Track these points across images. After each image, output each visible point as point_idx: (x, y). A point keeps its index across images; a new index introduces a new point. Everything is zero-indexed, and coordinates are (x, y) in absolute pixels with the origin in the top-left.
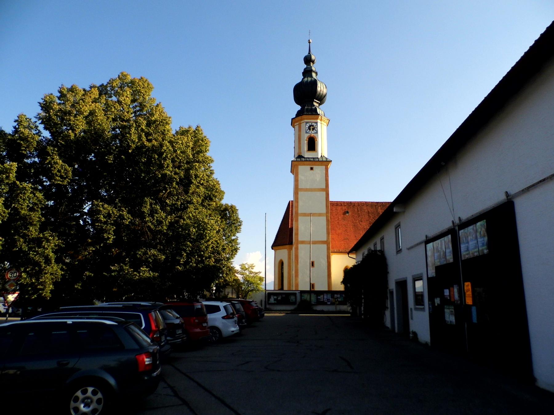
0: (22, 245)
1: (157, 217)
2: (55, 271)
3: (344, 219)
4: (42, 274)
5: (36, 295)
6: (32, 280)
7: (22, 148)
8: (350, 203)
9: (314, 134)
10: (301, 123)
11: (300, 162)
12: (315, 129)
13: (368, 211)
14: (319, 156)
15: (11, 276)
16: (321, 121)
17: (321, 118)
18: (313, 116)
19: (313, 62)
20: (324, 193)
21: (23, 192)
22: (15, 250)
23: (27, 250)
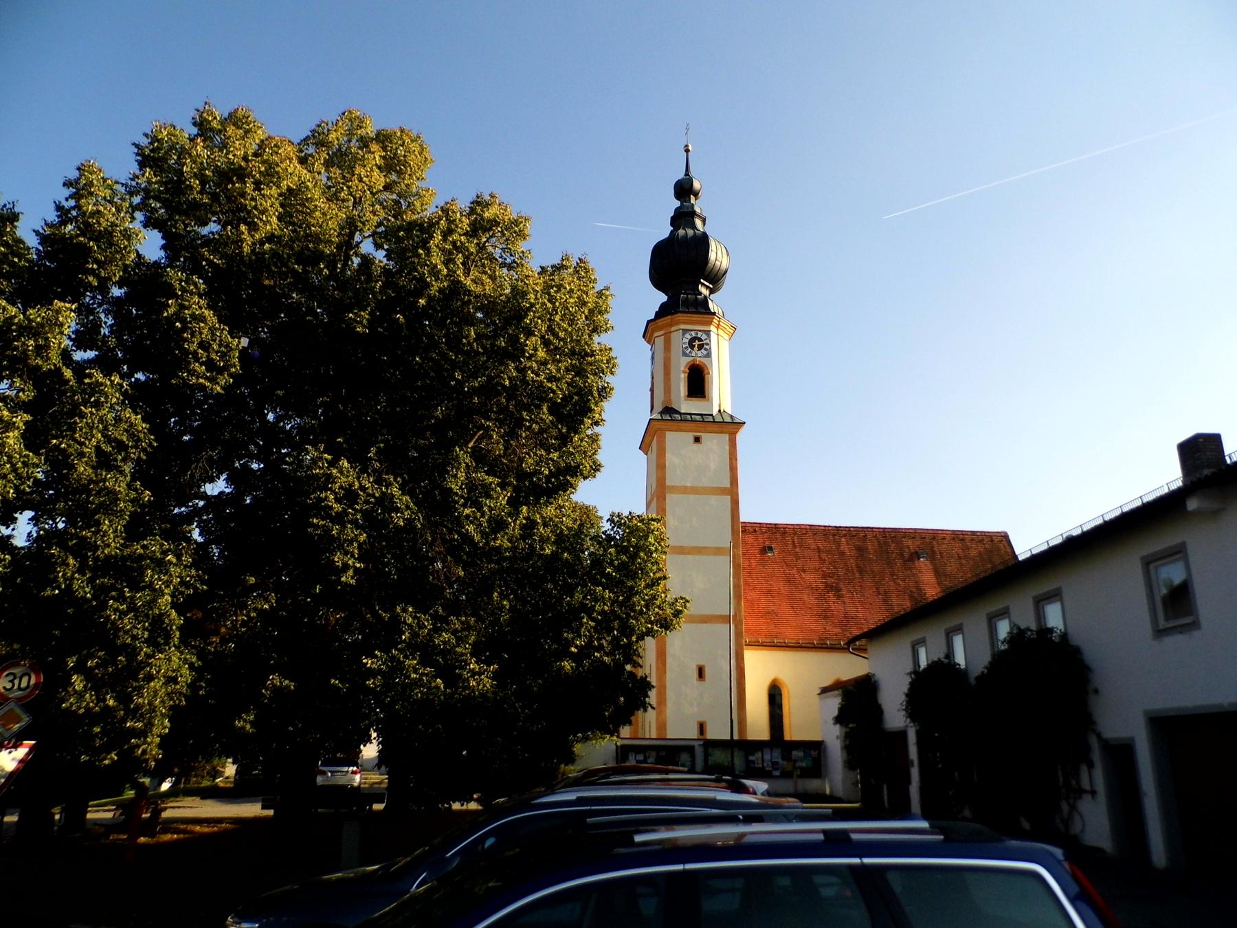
0: (72, 578)
1: (491, 509)
2: (174, 671)
4: (137, 680)
5: (115, 752)
6: (104, 700)
7: (88, 263)
8: (773, 526)
9: (702, 359)
10: (671, 332)
11: (670, 423)
12: (705, 346)
14: (715, 412)
15: (9, 686)
17: (719, 322)
18: (696, 317)
19: (696, 195)
21: (93, 399)
22: (48, 596)
23: (88, 595)
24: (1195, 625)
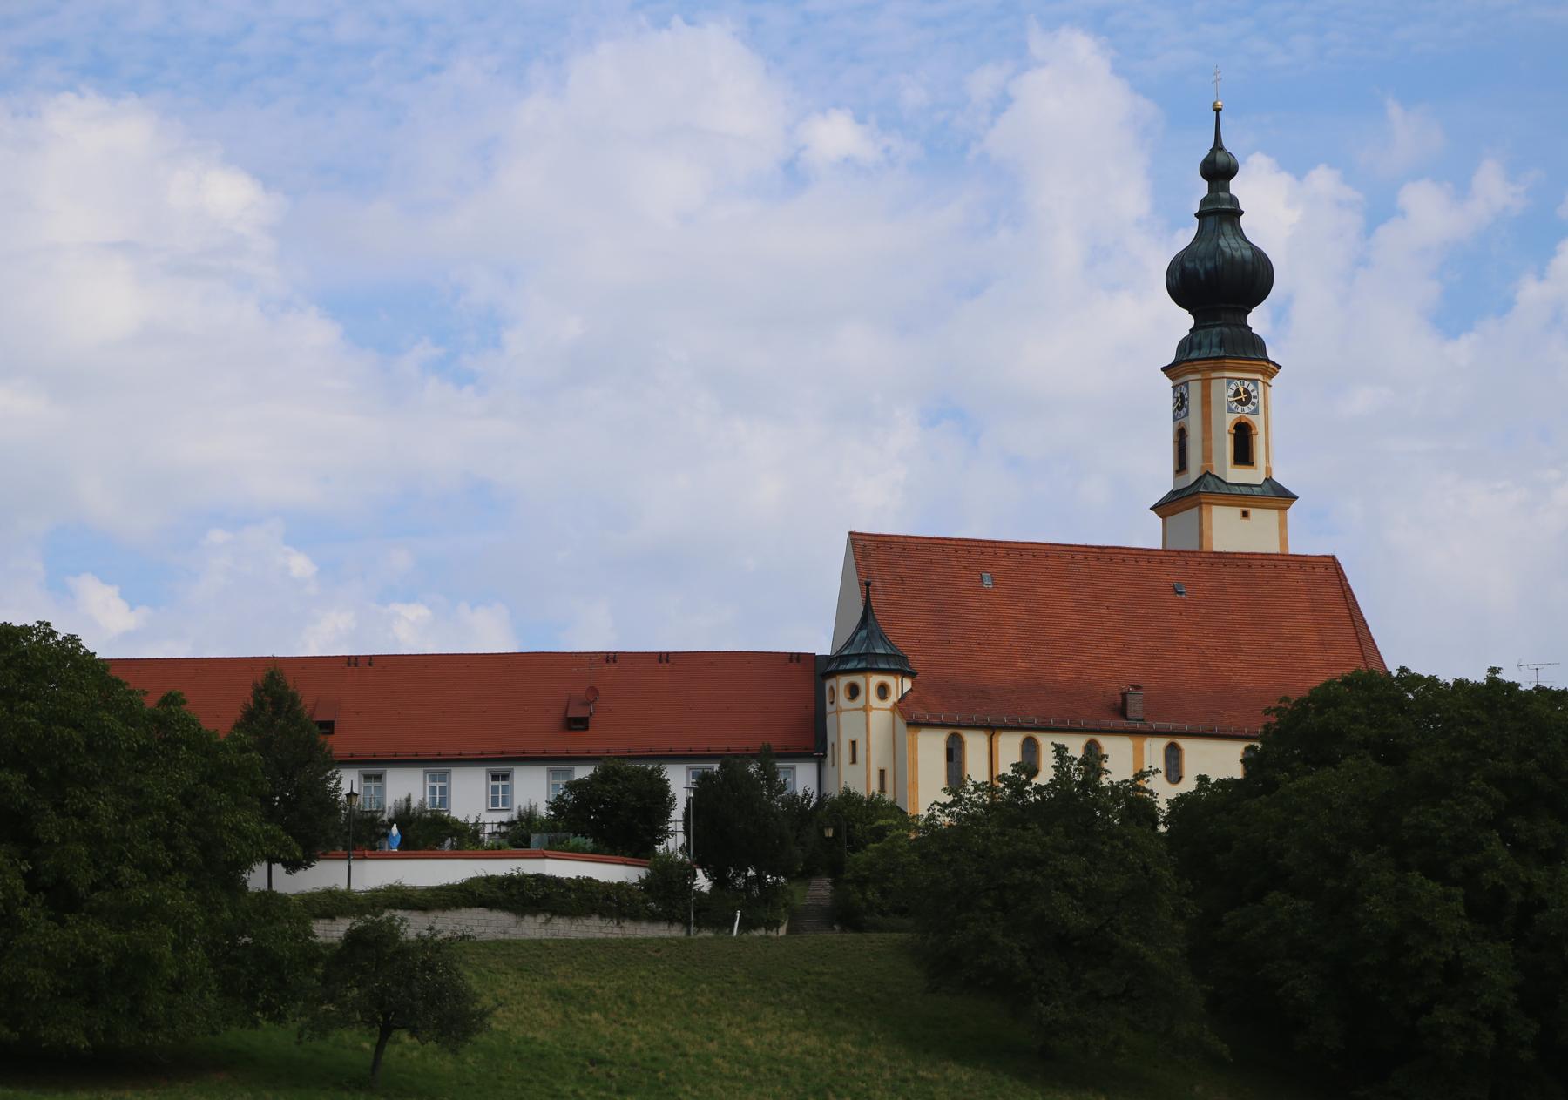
24: (851, 533)
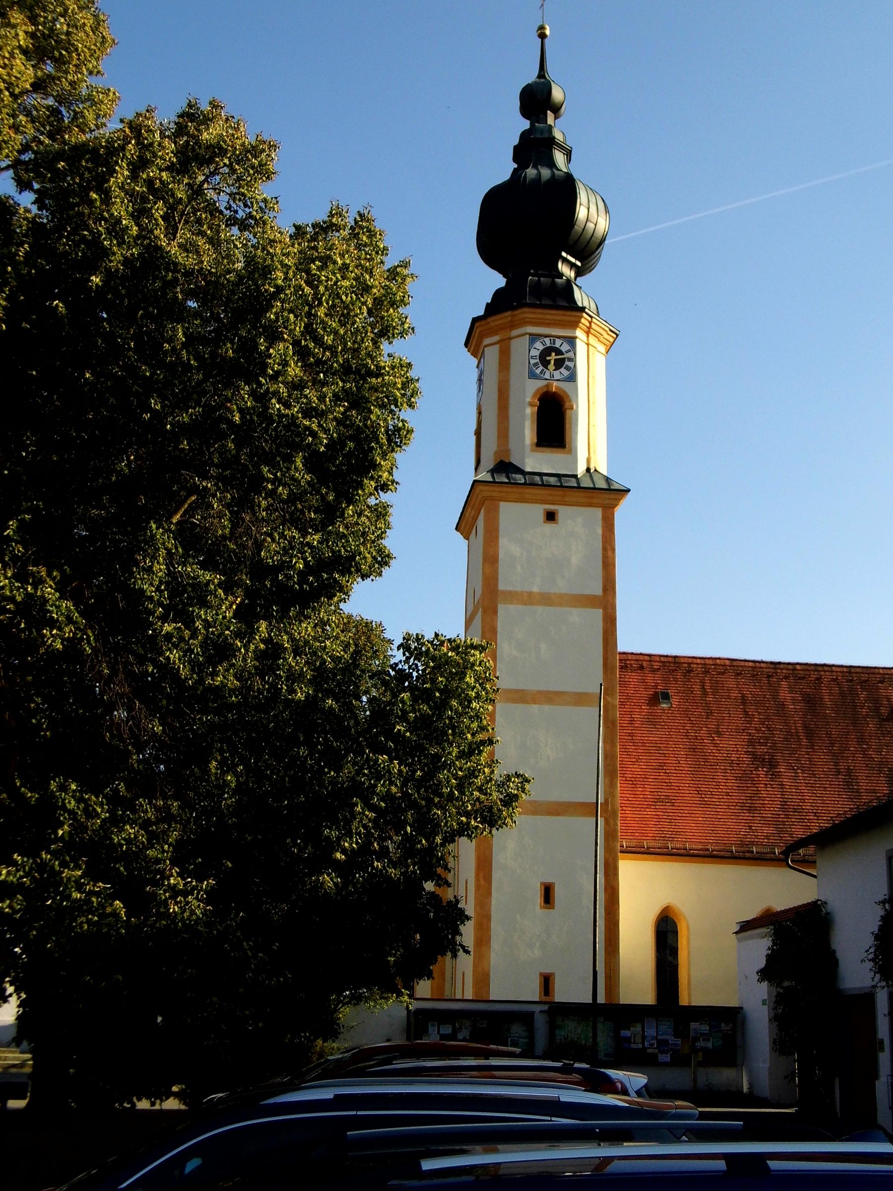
1: (207, 624)
3: (652, 721)
9: (560, 384)
10: (510, 339)
11: (506, 489)
12: (567, 363)
13: (743, 697)
14: (581, 470)
16: (588, 333)
17: (590, 323)
19: (556, 110)
20: (598, 614)
